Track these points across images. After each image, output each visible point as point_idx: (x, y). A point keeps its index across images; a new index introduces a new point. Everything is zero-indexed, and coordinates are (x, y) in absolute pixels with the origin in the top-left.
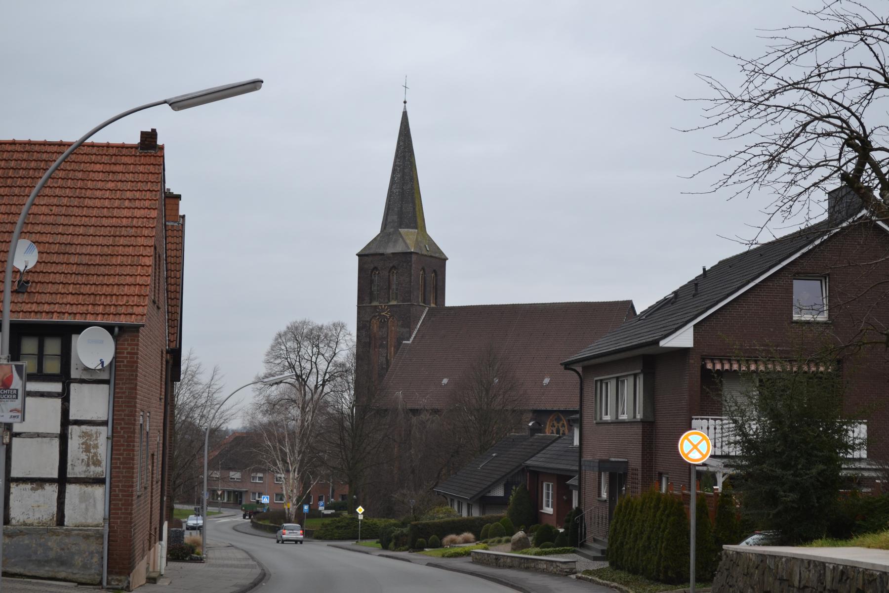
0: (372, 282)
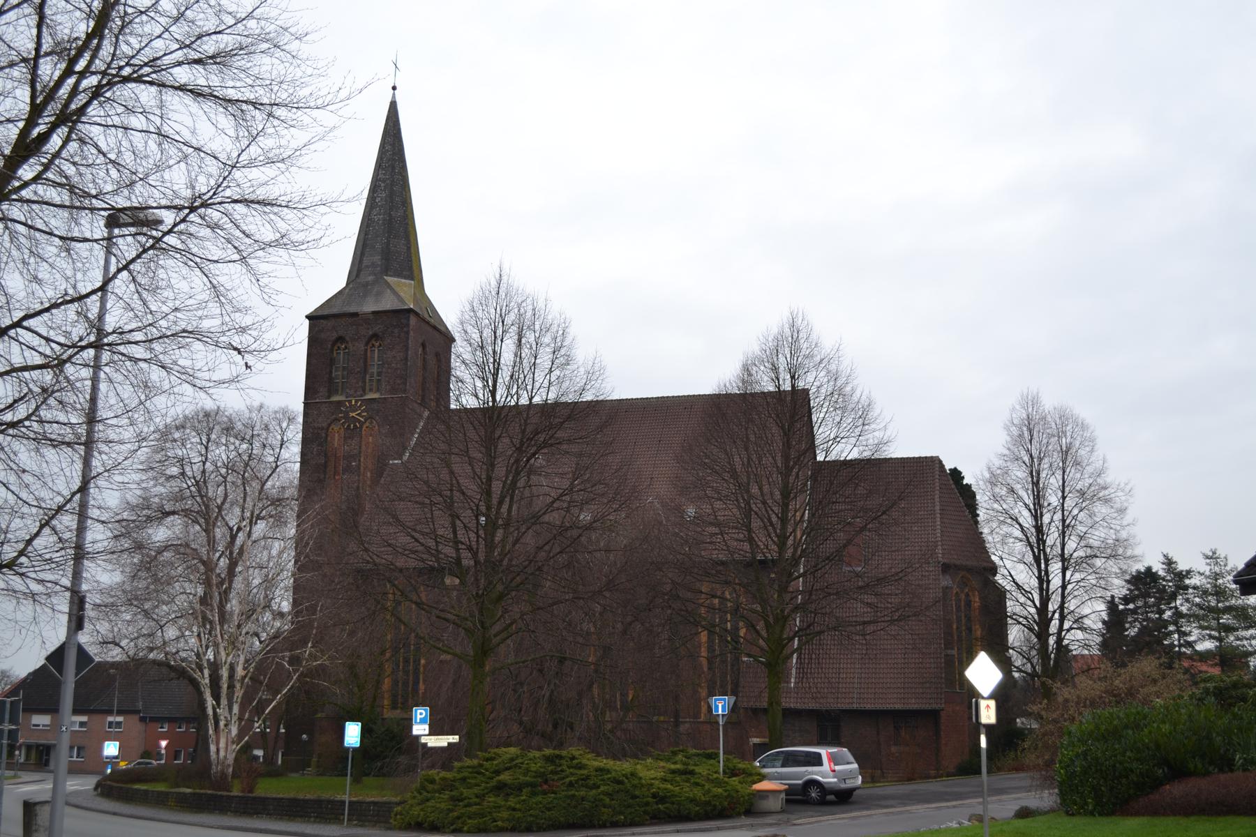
0: (332, 362)
